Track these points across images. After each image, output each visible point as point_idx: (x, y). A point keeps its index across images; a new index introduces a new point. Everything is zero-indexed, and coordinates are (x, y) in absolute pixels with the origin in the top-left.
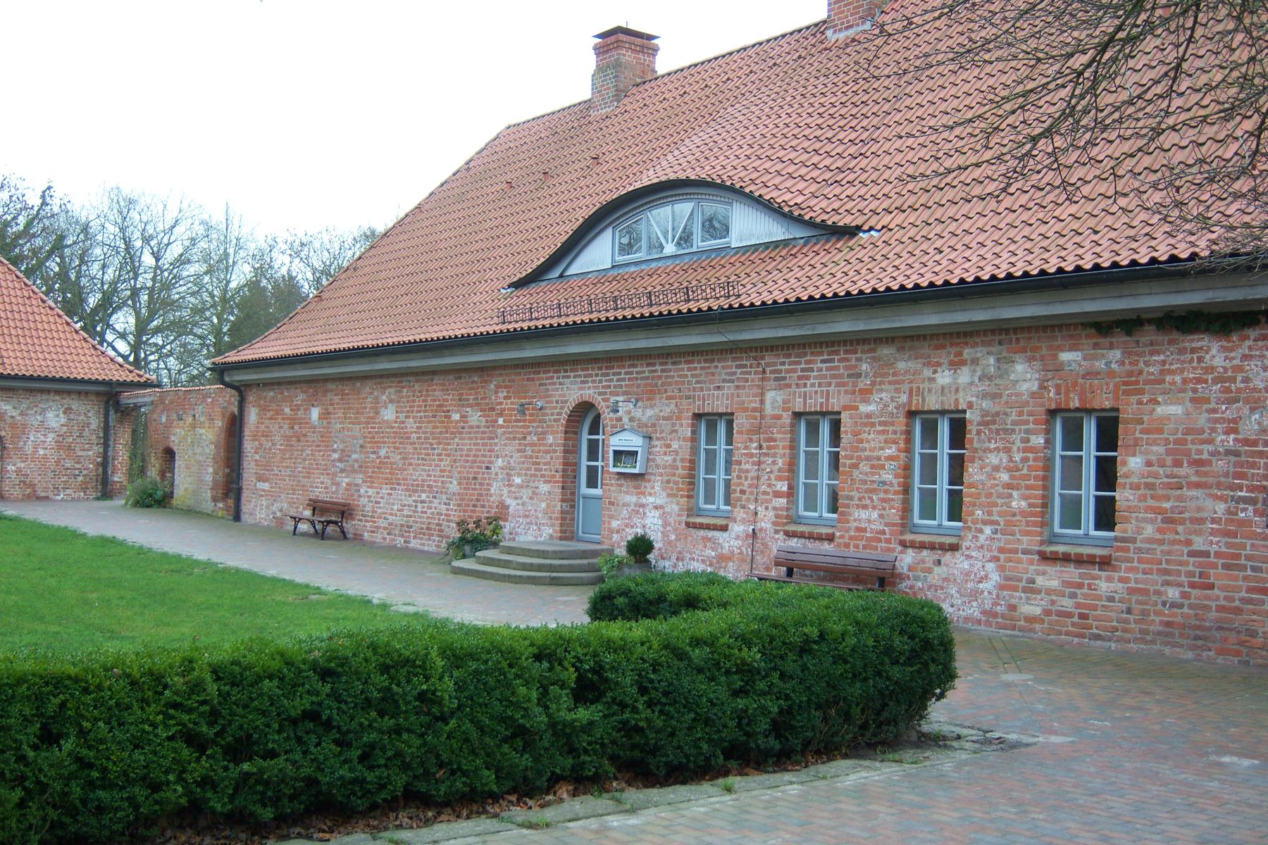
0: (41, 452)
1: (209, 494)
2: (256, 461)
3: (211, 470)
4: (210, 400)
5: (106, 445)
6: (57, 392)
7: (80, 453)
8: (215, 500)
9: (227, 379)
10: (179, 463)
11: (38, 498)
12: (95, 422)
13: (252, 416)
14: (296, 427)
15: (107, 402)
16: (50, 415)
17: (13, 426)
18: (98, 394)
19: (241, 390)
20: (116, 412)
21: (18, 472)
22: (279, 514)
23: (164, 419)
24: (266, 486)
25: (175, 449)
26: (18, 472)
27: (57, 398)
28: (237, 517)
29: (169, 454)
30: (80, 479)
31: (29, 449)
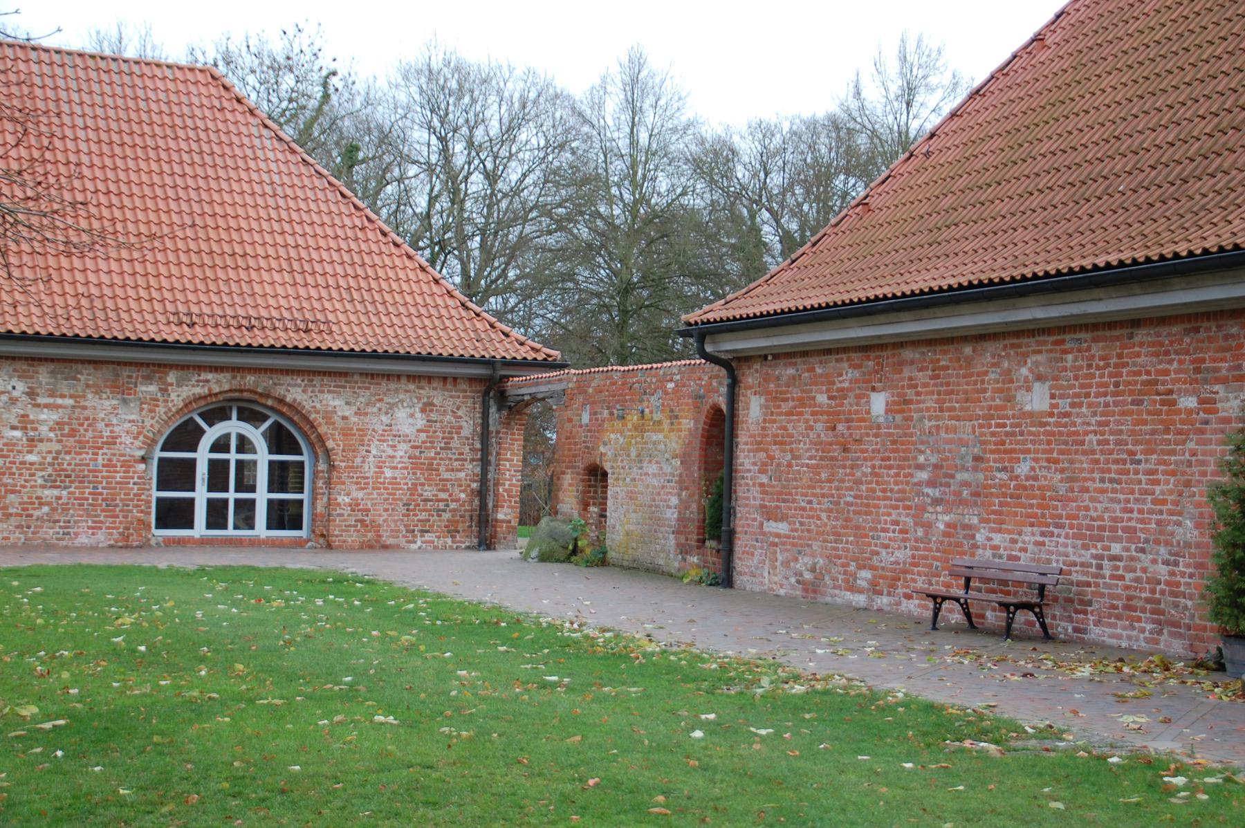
0: (388, 473)
1: (672, 541)
2: (762, 485)
3: (674, 501)
4: (671, 386)
5: (485, 462)
6: (412, 377)
7: (447, 475)
8: (683, 550)
9: (709, 348)
10: (615, 490)
11: (385, 547)
12: (468, 426)
13: (753, 409)
14: (840, 427)
15: (486, 394)
16: (401, 414)
17: (347, 433)
18: (472, 380)
19: (732, 366)
20: (499, 410)
21: (354, 506)
22: (808, 576)
23: (586, 418)
24: (783, 528)
25: (607, 466)
26: (354, 506)
27: (411, 387)
28: (725, 578)
29: (596, 476)
30: (446, 516)
31: (370, 469)
